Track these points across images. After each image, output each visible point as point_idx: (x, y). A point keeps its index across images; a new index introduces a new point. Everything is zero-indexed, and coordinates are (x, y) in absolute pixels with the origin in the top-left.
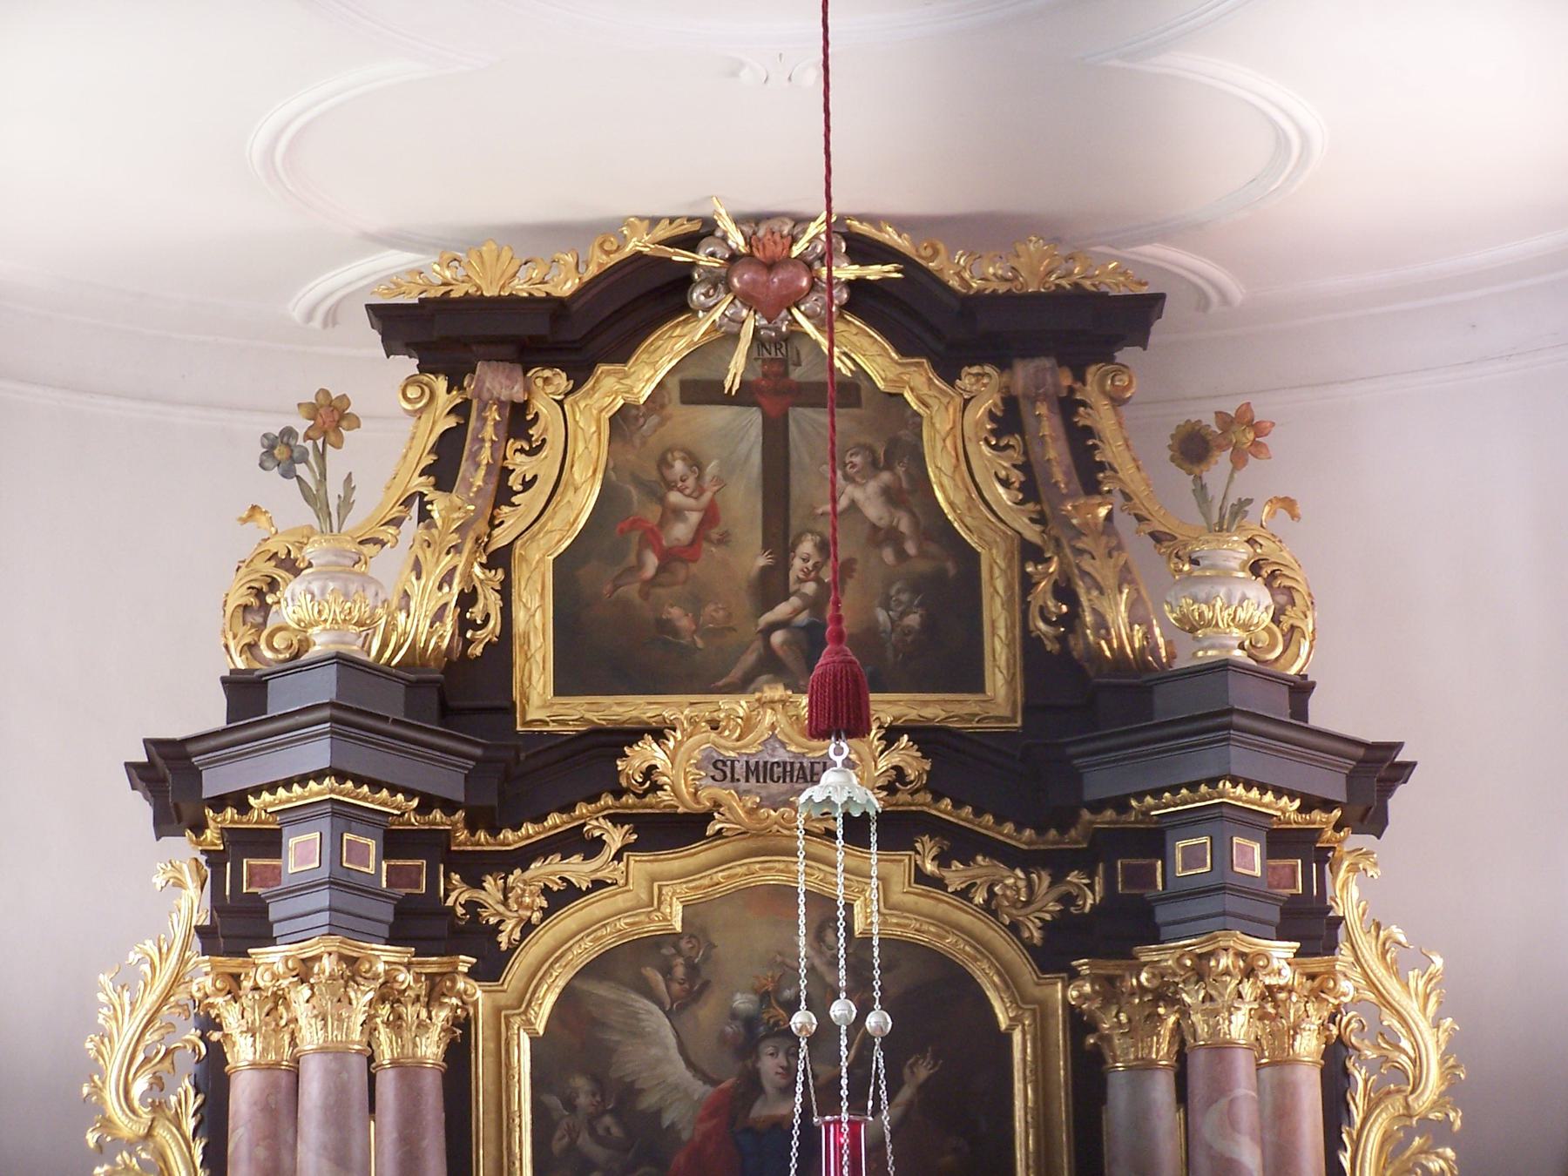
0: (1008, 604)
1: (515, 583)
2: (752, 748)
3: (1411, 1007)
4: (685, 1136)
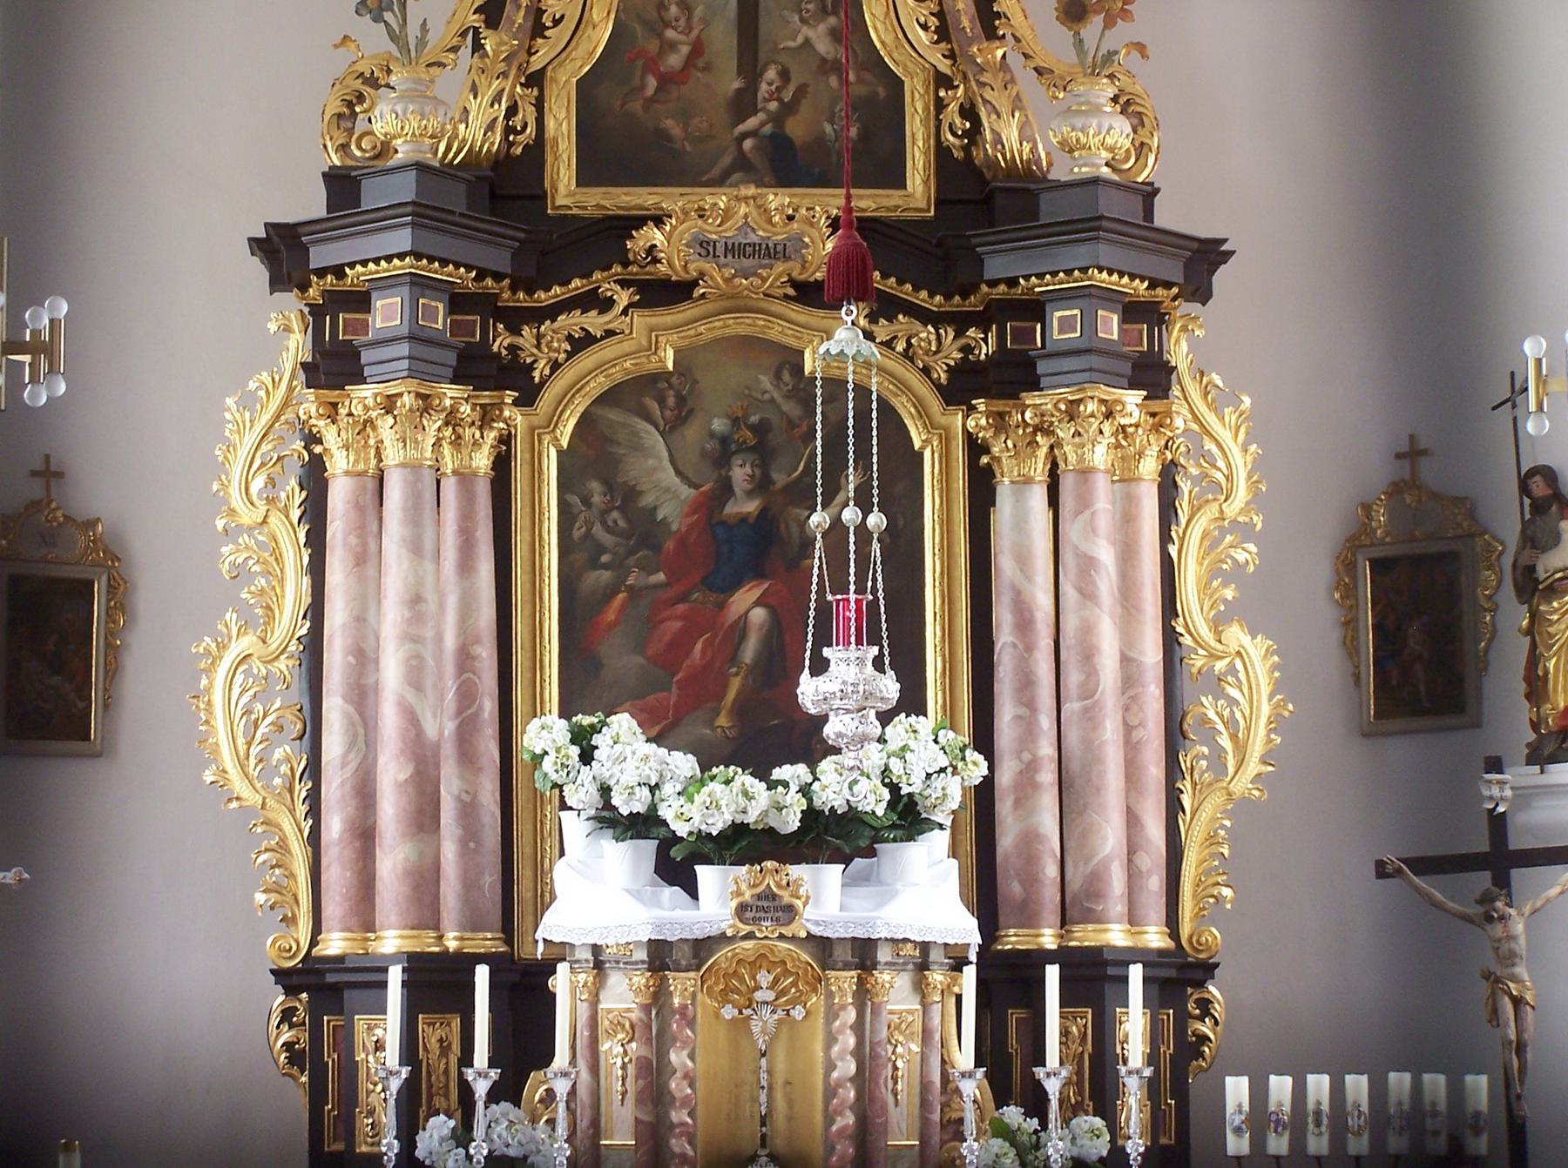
0: (925, 122)
1: (547, 98)
2: (730, 232)
3: (1225, 435)
4: (674, 527)
